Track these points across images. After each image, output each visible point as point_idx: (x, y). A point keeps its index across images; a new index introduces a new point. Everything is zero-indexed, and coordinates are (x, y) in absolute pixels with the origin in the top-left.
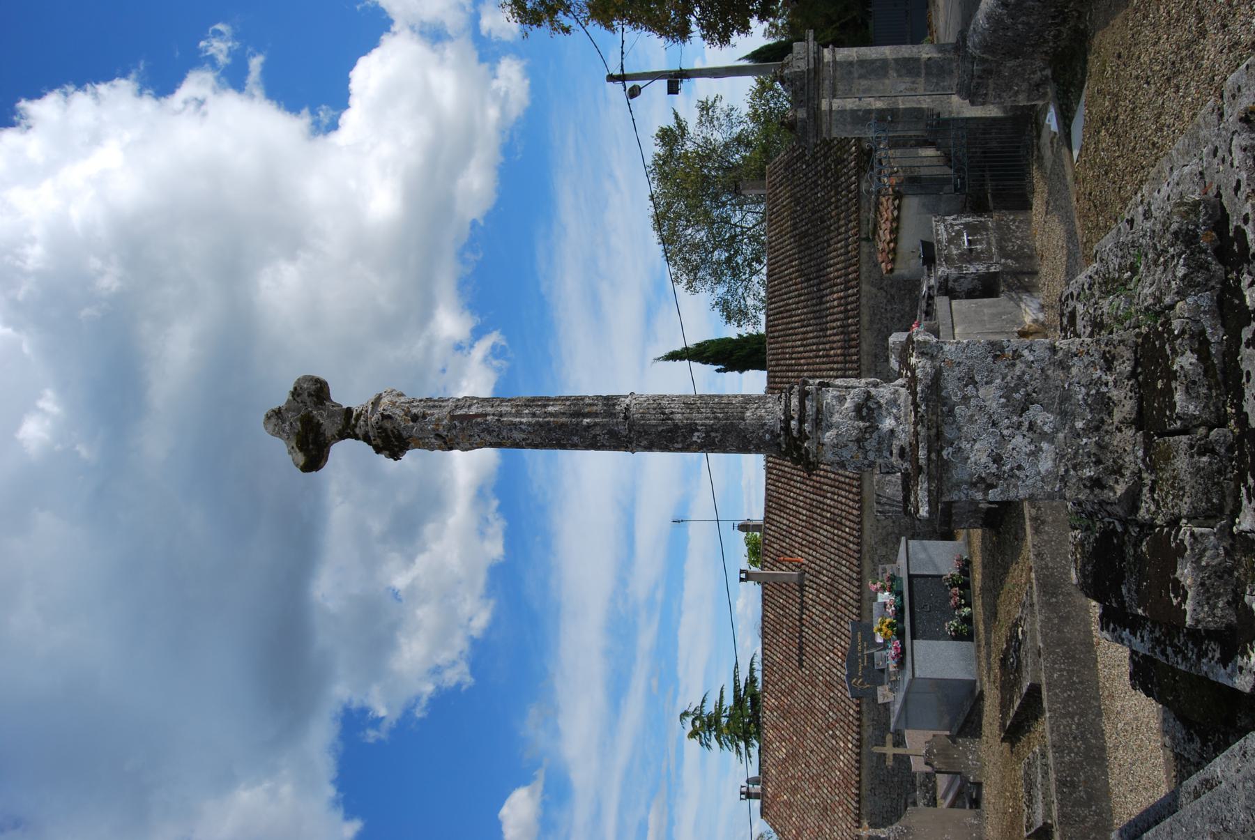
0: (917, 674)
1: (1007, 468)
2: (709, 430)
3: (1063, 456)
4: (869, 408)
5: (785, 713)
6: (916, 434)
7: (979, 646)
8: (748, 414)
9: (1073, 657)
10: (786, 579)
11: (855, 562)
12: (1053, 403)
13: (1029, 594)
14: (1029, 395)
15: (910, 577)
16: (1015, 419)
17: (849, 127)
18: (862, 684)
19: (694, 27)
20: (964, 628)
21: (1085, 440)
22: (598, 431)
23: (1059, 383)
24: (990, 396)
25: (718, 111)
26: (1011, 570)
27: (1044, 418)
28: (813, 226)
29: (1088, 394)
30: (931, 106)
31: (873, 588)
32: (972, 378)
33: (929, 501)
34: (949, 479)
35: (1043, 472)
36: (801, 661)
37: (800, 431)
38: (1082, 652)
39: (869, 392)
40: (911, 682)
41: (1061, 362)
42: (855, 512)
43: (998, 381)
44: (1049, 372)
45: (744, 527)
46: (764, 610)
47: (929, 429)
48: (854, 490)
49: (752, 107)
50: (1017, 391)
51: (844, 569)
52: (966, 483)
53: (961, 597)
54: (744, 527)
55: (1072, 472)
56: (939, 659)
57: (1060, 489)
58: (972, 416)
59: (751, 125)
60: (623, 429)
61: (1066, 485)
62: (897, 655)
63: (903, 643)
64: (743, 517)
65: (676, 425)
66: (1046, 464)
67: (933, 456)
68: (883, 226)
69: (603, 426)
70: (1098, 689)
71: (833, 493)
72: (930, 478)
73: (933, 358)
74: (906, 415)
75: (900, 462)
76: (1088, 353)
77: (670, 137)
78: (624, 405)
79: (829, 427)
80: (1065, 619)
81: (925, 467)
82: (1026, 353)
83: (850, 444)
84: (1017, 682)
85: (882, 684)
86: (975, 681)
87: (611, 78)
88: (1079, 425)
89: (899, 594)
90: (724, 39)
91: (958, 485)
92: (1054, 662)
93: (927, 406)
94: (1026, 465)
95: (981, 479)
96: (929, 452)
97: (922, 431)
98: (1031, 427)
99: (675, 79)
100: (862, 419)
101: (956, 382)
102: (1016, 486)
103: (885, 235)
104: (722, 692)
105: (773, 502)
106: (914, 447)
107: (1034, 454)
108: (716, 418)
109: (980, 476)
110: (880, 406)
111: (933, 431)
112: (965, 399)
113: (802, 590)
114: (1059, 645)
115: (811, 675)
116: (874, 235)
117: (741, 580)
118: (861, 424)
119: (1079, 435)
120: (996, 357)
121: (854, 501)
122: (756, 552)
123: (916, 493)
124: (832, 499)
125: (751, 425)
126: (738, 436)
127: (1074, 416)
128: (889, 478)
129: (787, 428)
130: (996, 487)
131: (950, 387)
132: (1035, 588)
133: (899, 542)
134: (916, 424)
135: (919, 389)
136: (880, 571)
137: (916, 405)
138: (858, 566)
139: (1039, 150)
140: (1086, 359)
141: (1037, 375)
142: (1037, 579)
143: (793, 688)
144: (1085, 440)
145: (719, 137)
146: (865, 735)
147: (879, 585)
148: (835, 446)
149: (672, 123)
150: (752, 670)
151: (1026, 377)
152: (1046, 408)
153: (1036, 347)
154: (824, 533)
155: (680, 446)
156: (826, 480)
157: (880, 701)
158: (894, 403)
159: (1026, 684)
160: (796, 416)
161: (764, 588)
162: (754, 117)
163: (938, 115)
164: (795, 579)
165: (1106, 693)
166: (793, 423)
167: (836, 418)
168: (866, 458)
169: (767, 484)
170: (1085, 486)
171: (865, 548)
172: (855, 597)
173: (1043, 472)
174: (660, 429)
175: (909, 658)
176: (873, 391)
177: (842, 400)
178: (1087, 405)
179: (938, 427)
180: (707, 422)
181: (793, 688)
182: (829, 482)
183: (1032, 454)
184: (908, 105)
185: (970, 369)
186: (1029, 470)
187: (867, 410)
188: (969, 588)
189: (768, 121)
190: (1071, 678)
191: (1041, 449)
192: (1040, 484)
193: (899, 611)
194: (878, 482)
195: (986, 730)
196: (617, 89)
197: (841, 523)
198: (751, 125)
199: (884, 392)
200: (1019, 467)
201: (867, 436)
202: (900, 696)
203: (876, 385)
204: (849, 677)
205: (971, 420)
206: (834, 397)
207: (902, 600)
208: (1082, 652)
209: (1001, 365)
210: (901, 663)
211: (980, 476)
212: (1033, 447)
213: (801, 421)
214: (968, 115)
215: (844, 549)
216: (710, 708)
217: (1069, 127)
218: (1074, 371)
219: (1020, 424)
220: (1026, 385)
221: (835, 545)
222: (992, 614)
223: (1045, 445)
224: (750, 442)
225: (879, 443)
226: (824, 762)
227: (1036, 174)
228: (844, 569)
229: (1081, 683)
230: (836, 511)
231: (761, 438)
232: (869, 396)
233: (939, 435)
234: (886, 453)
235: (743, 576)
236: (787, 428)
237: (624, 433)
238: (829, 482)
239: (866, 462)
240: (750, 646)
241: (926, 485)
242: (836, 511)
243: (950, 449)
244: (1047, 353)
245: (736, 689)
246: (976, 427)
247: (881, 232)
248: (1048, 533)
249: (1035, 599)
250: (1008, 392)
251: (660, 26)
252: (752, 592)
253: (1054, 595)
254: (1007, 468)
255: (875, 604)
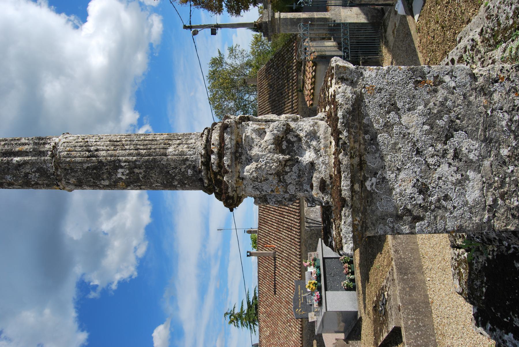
0: (328, 310)
1: (433, 199)
2: (133, 166)
3: (490, 185)
4: (289, 142)
5: (269, 315)
6: (338, 163)
7: (359, 293)
8: (171, 150)
9: (419, 311)
10: (268, 255)
11: (298, 247)
12: (477, 129)
13: (391, 273)
14: (452, 121)
15: (324, 259)
16: (439, 146)
17: (289, 27)
18: (301, 312)
19: (224, 7)
20: (351, 285)
21: (511, 168)
22: (27, 169)
23: (481, 109)
24: (413, 121)
25: (237, 51)
26: (377, 257)
27: (469, 145)
28: (278, 97)
29: (511, 120)
30: (331, 17)
31: (305, 264)
32: (394, 104)
33: (354, 237)
34: (373, 212)
35: (471, 203)
36: (275, 291)
37: (220, 165)
38: (423, 307)
39: (288, 124)
40: (325, 313)
41: (482, 89)
42: (297, 224)
43: (421, 107)
44: (472, 98)
45: (249, 232)
46: (259, 268)
47: (351, 157)
48: (297, 214)
49: (252, 48)
50: (441, 118)
51: (293, 250)
52: (391, 216)
53: (349, 268)
54: (249, 232)
55: (500, 202)
56: (340, 301)
57: (489, 220)
58: (396, 144)
59: (252, 57)
60: (51, 167)
61: (494, 216)
62: (318, 299)
63: (321, 293)
64: (248, 228)
65: (100, 162)
66: (473, 194)
67: (357, 187)
68: (308, 82)
69: (33, 164)
70: (433, 329)
71: (288, 216)
72: (355, 212)
73: (353, 84)
74: (326, 147)
75: (321, 195)
76: (508, 79)
77: (217, 62)
78: (53, 144)
79: (249, 160)
80: (412, 288)
81: (348, 199)
82: (447, 79)
83: (271, 178)
84: (384, 323)
85: (311, 311)
86: (357, 312)
87: (185, 27)
88: (505, 152)
89: (318, 267)
90: (238, 13)
91: (383, 218)
92: (408, 314)
93: (348, 131)
94: (452, 195)
95: (409, 212)
96: (353, 182)
97: (345, 160)
98: (456, 156)
99: (214, 29)
100: (282, 152)
101: (377, 109)
102: (443, 217)
103: (308, 86)
104: (242, 303)
105: (262, 221)
106: (336, 179)
107: (462, 182)
108: (138, 154)
109: (405, 208)
110: (300, 139)
111: (357, 160)
112: (388, 126)
113: (275, 260)
114: (410, 304)
115: (280, 298)
116: (303, 87)
117: (248, 256)
118: (281, 157)
119: (504, 163)
120: (417, 83)
121: (297, 219)
122: (255, 243)
123: (338, 228)
124: (287, 219)
125: (174, 161)
126: (161, 172)
127: (499, 143)
128: (312, 209)
129: (207, 163)
130: (422, 219)
131: (372, 114)
132: (395, 270)
133: (318, 240)
134: (337, 153)
135: (340, 114)
136: (309, 255)
137: (336, 133)
138: (299, 249)
139: (386, 38)
140: (507, 85)
141: (459, 102)
142: (396, 265)
143: (272, 303)
144: (511, 168)
145: (238, 62)
146: (304, 325)
147: (308, 263)
148: (255, 179)
149: (217, 55)
150: (255, 294)
151: (449, 103)
152: (470, 135)
153: (458, 74)
154: (284, 234)
155: (107, 183)
156: (284, 210)
157: (310, 320)
158: (313, 135)
159: (391, 328)
160: (215, 150)
161: (258, 259)
162: (253, 53)
163: (335, 21)
164: (272, 255)
165: (439, 332)
166: (213, 157)
167: (255, 151)
168: (286, 192)
169: (259, 212)
170: (513, 216)
171: (302, 240)
172: (298, 263)
173: (471, 203)
174: (85, 166)
175: (324, 301)
176: (293, 125)
177: (261, 133)
178: (511, 131)
179: (360, 156)
180: (130, 158)
181: (272, 303)
182: (286, 211)
183: (459, 183)
184: (319, 17)
185: (392, 95)
186: (457, 202)
187: (287, 143)
188: (353, 263)
189: (259, 55)
190: (418, 323)
191: (467, 178)
192: (468, 215)
193: (318, 278)
194: (307, 211)
195: (363, 336)
196: (190, 32)
197: (291, 229)
198: (252, 57)
199: (305, 125)
200: (446, 198)
201: (287, 169)
202: (320, 319)
203: (295, 120)
204: (295, 308)
205: (395, 148)
206: (254, 130)
207: (320, 269)
208: (423, 307)
209: (423, 92)
210: (320, 304)
211: (405, 208)
212: (459, 176)
213: (221, 155)
214: (350, 21)
215: (293, 241)
216: (237, 311)
217: (411, 4)
218: (496, 97)
219: (445, 153)
220: (449, 111)
221: (289, 239)
222: (365, 278)
223: (471, 174)
224: (173, 178)
225: (299, 176)
226: (286, 337)
227: (384, 50)
228: (293, 250)
229: (424, 326)
230: (289, 224)
231: (183, 174)
232: (288, 130)
233: (362, 164)
234: (307, 187)
235: (249, 254)
236: (207, 163)
237: (52, 171)
238: (286, 211)
239: (287, 196)
240: (253, 283)
241: (350, 219)
242: (289, 224)
243: (374, 180)
244: (468, 79)
245: (248, 303)
246: (400, 156)
247: (307, 85)
248: (400, 239)
249: (395, 277)
250: (431, 119)
251: (209, 7)
252: (254, 259)
253: (406, 274)
254: (433, 199)
255: (306, 273)
